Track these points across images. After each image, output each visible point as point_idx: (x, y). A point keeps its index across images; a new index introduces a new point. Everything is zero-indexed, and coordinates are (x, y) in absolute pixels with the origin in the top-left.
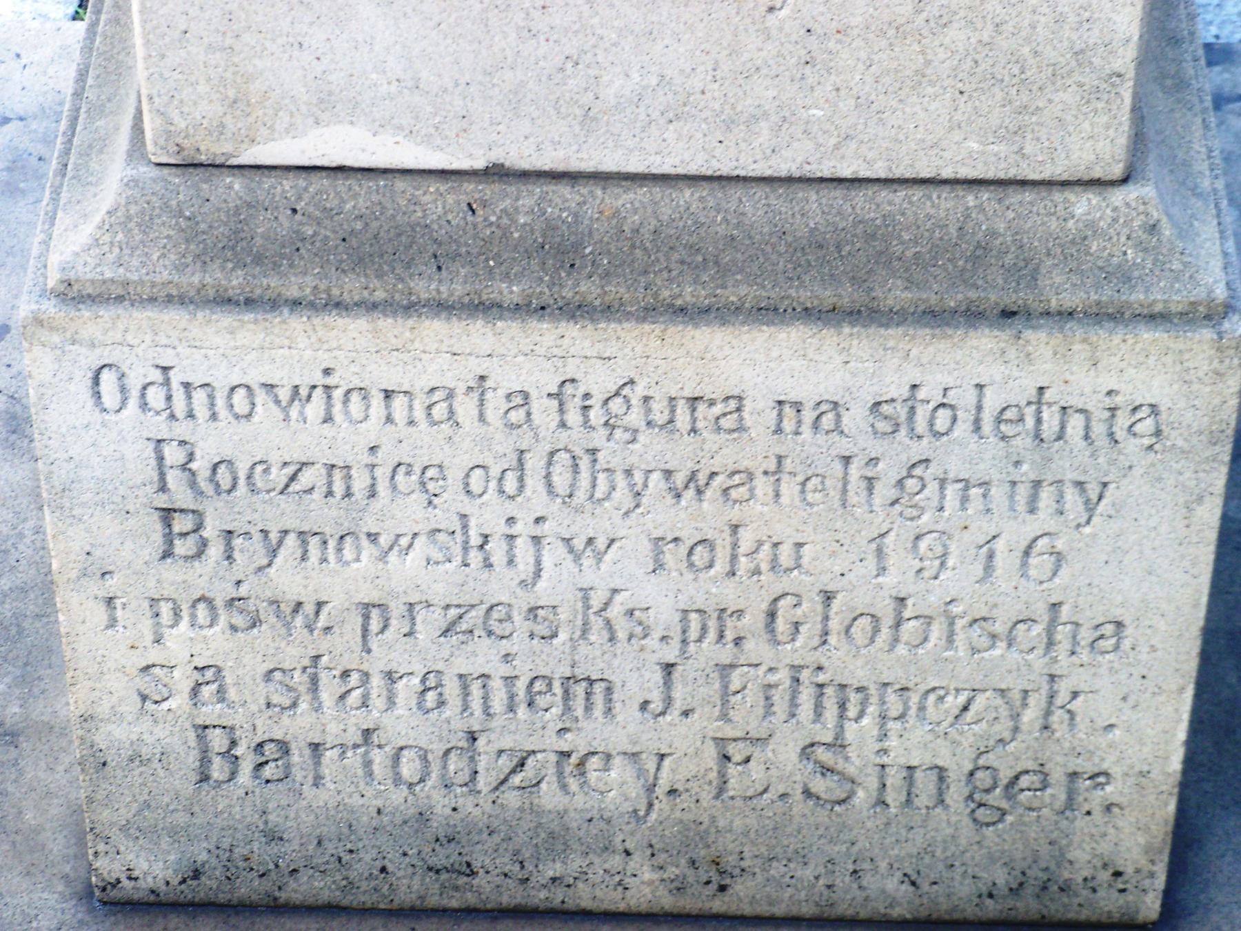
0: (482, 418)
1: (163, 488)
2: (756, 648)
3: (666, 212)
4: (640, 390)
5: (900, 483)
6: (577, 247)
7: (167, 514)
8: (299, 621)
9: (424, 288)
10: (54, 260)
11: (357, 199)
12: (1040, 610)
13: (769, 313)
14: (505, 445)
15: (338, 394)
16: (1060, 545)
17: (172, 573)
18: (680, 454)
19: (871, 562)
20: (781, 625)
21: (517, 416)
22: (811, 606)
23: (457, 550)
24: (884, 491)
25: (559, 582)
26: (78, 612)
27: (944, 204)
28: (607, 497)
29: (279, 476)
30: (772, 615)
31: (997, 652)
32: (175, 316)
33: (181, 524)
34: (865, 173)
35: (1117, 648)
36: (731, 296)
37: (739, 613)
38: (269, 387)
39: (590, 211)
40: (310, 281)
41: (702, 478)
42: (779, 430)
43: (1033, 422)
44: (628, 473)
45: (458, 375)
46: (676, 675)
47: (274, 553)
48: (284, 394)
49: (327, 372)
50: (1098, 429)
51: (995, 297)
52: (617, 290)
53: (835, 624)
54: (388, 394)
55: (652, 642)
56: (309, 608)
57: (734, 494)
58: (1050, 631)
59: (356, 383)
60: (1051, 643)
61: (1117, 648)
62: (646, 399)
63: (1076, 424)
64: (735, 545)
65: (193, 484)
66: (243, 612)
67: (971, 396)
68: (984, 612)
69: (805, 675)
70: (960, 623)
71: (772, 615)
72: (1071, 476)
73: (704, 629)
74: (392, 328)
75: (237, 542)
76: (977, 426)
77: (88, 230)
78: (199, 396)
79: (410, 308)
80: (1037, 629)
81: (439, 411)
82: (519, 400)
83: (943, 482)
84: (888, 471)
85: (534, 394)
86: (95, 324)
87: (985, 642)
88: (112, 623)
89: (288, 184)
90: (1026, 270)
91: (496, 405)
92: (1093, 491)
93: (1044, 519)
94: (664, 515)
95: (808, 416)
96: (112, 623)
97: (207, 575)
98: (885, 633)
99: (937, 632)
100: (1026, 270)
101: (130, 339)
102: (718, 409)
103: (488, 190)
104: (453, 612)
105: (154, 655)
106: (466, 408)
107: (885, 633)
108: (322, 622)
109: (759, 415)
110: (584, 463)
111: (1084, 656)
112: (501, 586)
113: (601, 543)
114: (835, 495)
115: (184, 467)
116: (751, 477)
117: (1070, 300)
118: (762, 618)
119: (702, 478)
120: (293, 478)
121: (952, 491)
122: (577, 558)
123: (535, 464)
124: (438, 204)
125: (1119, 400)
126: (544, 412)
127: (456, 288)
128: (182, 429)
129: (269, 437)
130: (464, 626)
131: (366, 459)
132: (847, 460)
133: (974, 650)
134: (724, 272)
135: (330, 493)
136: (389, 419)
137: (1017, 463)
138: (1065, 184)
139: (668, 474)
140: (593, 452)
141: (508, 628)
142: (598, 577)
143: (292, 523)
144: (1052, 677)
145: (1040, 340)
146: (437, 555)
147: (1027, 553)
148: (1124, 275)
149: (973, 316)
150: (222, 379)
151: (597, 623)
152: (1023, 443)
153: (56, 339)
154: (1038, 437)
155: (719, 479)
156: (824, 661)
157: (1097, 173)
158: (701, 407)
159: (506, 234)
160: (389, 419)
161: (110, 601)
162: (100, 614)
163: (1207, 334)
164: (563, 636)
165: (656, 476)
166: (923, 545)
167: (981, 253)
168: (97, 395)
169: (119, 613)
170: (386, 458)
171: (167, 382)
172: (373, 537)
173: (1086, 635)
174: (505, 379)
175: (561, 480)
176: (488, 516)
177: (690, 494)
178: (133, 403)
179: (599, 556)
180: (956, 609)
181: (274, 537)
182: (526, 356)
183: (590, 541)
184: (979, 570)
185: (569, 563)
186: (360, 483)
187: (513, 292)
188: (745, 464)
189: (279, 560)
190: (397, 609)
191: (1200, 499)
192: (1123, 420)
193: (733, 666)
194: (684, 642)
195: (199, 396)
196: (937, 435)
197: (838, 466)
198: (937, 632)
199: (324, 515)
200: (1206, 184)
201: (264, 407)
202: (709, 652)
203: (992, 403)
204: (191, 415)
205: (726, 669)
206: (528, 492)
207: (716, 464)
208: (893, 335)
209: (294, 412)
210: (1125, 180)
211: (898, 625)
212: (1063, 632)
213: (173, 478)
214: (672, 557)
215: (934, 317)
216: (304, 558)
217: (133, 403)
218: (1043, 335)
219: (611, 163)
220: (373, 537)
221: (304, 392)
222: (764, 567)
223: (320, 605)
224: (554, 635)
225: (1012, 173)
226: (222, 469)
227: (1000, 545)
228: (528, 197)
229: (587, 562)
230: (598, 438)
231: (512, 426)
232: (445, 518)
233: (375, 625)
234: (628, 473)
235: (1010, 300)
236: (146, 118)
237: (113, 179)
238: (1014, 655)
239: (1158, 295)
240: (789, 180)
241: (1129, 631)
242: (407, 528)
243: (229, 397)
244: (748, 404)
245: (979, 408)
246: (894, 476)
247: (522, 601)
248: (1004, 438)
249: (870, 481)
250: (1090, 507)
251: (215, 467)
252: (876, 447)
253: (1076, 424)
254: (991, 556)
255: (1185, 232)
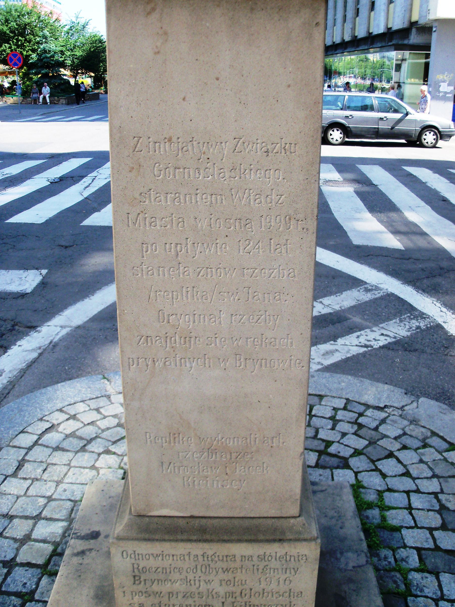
0: (189, 559)
1: (134, 571)
2: (239, 599)
3: (221, 523)
4: (217, 554)
5: (263, 569)
6: (206, 529)
7: (134, 577)
8: (157, 595)
9: (179, 537)
10: (116, 532)
11: (168, 521)
12: (288, 590)
13: (239, 541)
14: (194, 564)
15: (164, 555)
16: (291, 579)
17: (135, 587)
18: (225, 565)
19: (258, 583)
20: (243, 594)
21: (195, 559)
22: (248, 591)
23: (185, 582)
24: (260, 571)
25: (203, 587)
26: (118, 594)
27: (270, 522)
28: (212, 573)
29: (154, 570)
30: (241, 593)
31: (281, 598)
32: (136, 542)
33: (137, 578)
34: (255, 516)
35: (301, 596)
36: (233, 538)
37: (236, 593)
38: (152, 554)
39: (208, 523)
40: (159, 536)
41: (228, 569)
42: (242, 560)
43: (285, 559)
44: (215, 568)
45: (185, 552)
46: (225, 604)
47: (153, 583)
48: (155, 556)
49: (162, 552)
50: (296, 559)
51: (278, 537)
52: (213, 537)
53: (252, 594)
54: (173, 556)
55: (220, 598)
56: (159, 593)
57: (234, 572)
58: (290, 594)
59: (167, 553)
60: (290, 596)
61: (301, 596)
62: (218, 556)
63: (292, 559)
64: (235, 581)
65: (139, 571)
66: (148, 594)
67: (274, 554)
68: (278, 591)
69: (247, 603)
70: (274, 593)
71: (241, 593)
72: (292, 567)
73: (229, 596)
74: (174, 544)
75: (147, 581)
76: (276, 559)
77: (121, 527)
78: (140, 556)
79: (177, 541)
80: (288, 594)
81: (182, 558)
82: (196, 556)
83: (270, 569)
84: (261, 567)
85: (199, 555)
86: (122, 543)
87: (278, 596)
88: (124, 596)
89: (156, 519)
90: (283, 533)
91: (192, 557)
92: (296, 569)
93: (288, 574)
94: (221, 576)
95: (247, 558)
96: (124, 596)
97: (141, 587)
98: (261, 595)
99: (270, 595)
100: (283, 533)
101: (411, 342)
102: (231, 557)
103: (190, 520)
104: (185, 593)
105: (132, 602)
106: (187, 558)
107: (261, 595)
108: (162, 595)
109: (238, 558)
110: (208, 567)
111: (296, 598)
112: (193, 589)
113: (211, 581)
114: (252, 572)
115: (138, 568)
116: (237, 569)
117: (291, 537)
118: (239, 593)
119: (228, 569)
120: (157, 570)
121: (272, 570)
122: (207, 583)
123: (199, 567)
124: (182, 522)
125: (300, 554)
126: (201, 559)
127: (185, 537)
128: (137, 561)
129: (152, 563)
130: (187, 596)
131: (169, 567)
132: (254, 566)
133: (277, 598)
134: (231, 534)
135: (163, 573)
136: (173, 560)
137: (283, 565)
138: (289, 517)
139: (222, 569)
140: (209, 565)
141: (194, 596)
142: (210, 587)
143: (156, 578)
144: (290, 602)
145: (285, 544)
146: (182, 583)
147: (285, 580)
148: (300, 533)
149: (274, 541)
150: (144, 552)
151: (210, 595)
152: (284, 562)
153: (116, 546)
154: (286, 561)
155: (231, 569)
156: (251, 601)
157: (295, 515)
158: (228, 557)
159: (194, 527)
160: (173, 560)
161: (124, 592)
162: (123, 594)
163: (314, 542)
164: (204, 598)
165: (220, 569)
166: (267, 580)
167: (275, 530)
168: (123, 556)
169: (126, 594)
170: (173, 566)
171: (135, 553)
172: (170, 580)
173: (296, 594)
174: (194, 552)
175: (204, 570)
176: (191, 576)
177: (226, 572)
178: (129, 557)
179: (210, 584)
180: (274, 590)
181: (153, 580)
182: (197, 549)
183: (209, 581)
184: (277, 584)
185: (205, 584)
186: (168, 571)
187: (195, 538)
188: (236, 566)
189: (154, 584)
190: (175, 593)
191: (314, 570)
192: (300, 557)
193: (235, 602)
194: (226, 598)
195: (140, 556)
196: (269, 561)
197: (252, 567)
198: (270, 595)
199: (162, 577)
200: (313, 516)
201: (151, 557)
202: (230, 600)
203: (278, 555)
204: (139, 559)
205: (233, 603)
206: (198, 572)
207: (231, 566)
208: (261, 544)
209: (157, 559)
210: (299, 516)
211: (263, 593)
212: (292, 594)
213: (136, 570)
214: (224, 583)
215: (268, 541)
216: (158, 584)
217: (129, 557)
218: (286, 543)
219: (212, 514)
220: (170, 580)
221: (158, 555)
222: (240, 584)
223: (161, 593)
224: (203, 597)
225: (280, 516)
226: (144, 569)
227: (280, 579)
228: (197, 521)
229: (208, 584)
230: (210, 562)
231: (195, 561)
232: (183, 576)
233: (171, 596)
234: (215, 568)
235: (281, 537)
236: (132, 508)
237: (126, 518)
238: (284, 598)
239: (306, 536)
240: (243, 518)
241: (303, 593)
242: (176, 578)
243: (146, 556)
244: (236, 557)
245: (276, 556)
246: (262, 568)
247: (197, 592)
248: (281, 561)
249: (258, 569)
250: (296, 573)
251: (143, 568)
252: (259, 563)
253: (292, 559)
254: (279, 581)
255: (310, 525)
